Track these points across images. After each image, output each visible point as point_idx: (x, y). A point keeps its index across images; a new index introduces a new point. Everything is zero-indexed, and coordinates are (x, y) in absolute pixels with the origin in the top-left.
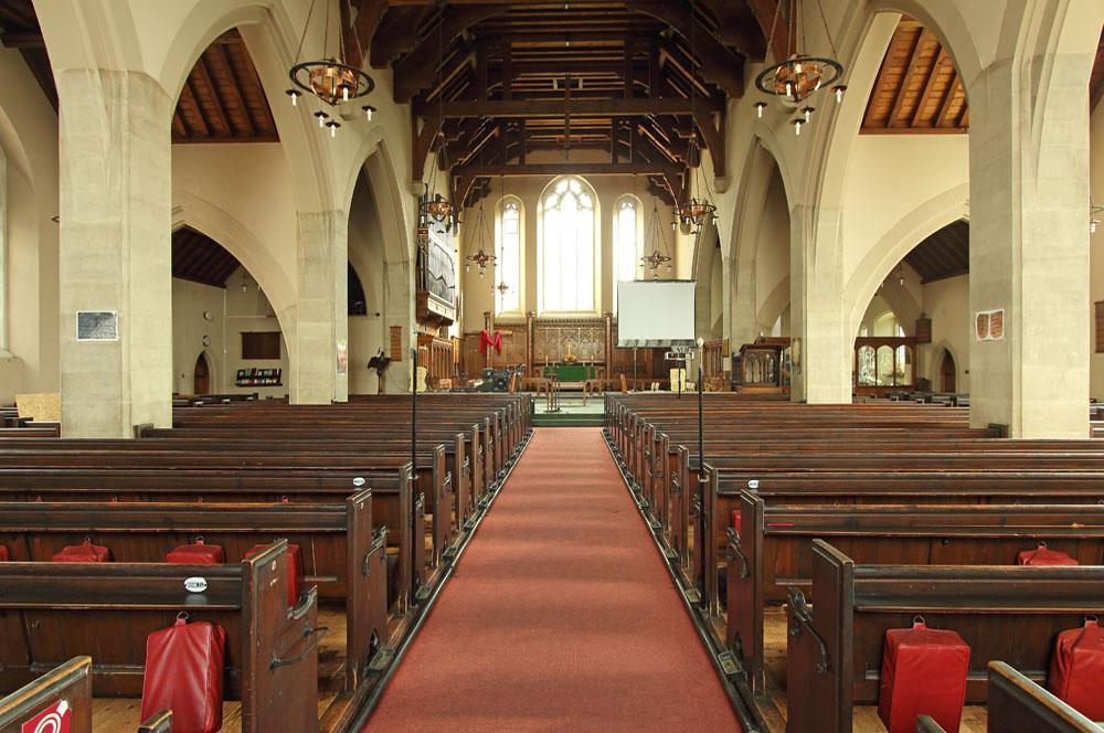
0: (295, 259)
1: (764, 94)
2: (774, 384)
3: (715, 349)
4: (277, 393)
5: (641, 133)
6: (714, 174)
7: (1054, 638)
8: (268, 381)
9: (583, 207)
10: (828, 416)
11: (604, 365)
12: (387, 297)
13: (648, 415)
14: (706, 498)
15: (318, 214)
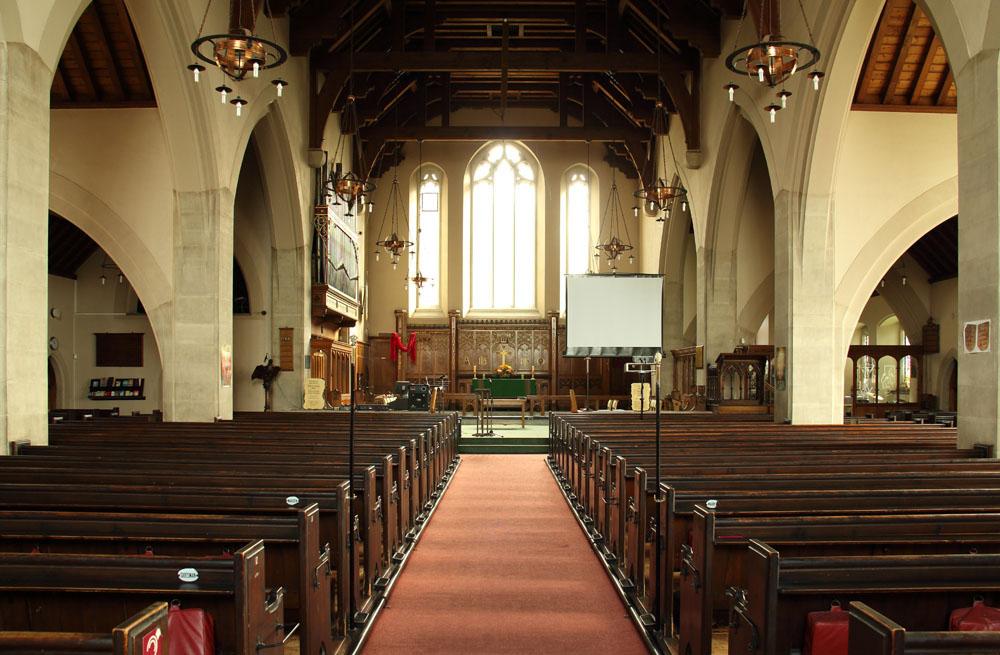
0: (171, 246)
1: (735, 74)
2: (757, 402)
3: (683, 358)
4: (145, 408)
5: (596, 91)
6: (685, 145)
7: (948, 615)
8: (128, 393)
9: (522, 179)
10: (817, 440)
11: (548, 377)
12: (275, 291)
13: (601, 438)
14: (663, 518)
15: (200, 193)
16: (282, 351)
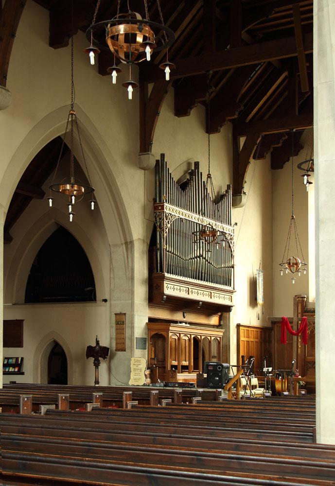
16: (117, 334)
